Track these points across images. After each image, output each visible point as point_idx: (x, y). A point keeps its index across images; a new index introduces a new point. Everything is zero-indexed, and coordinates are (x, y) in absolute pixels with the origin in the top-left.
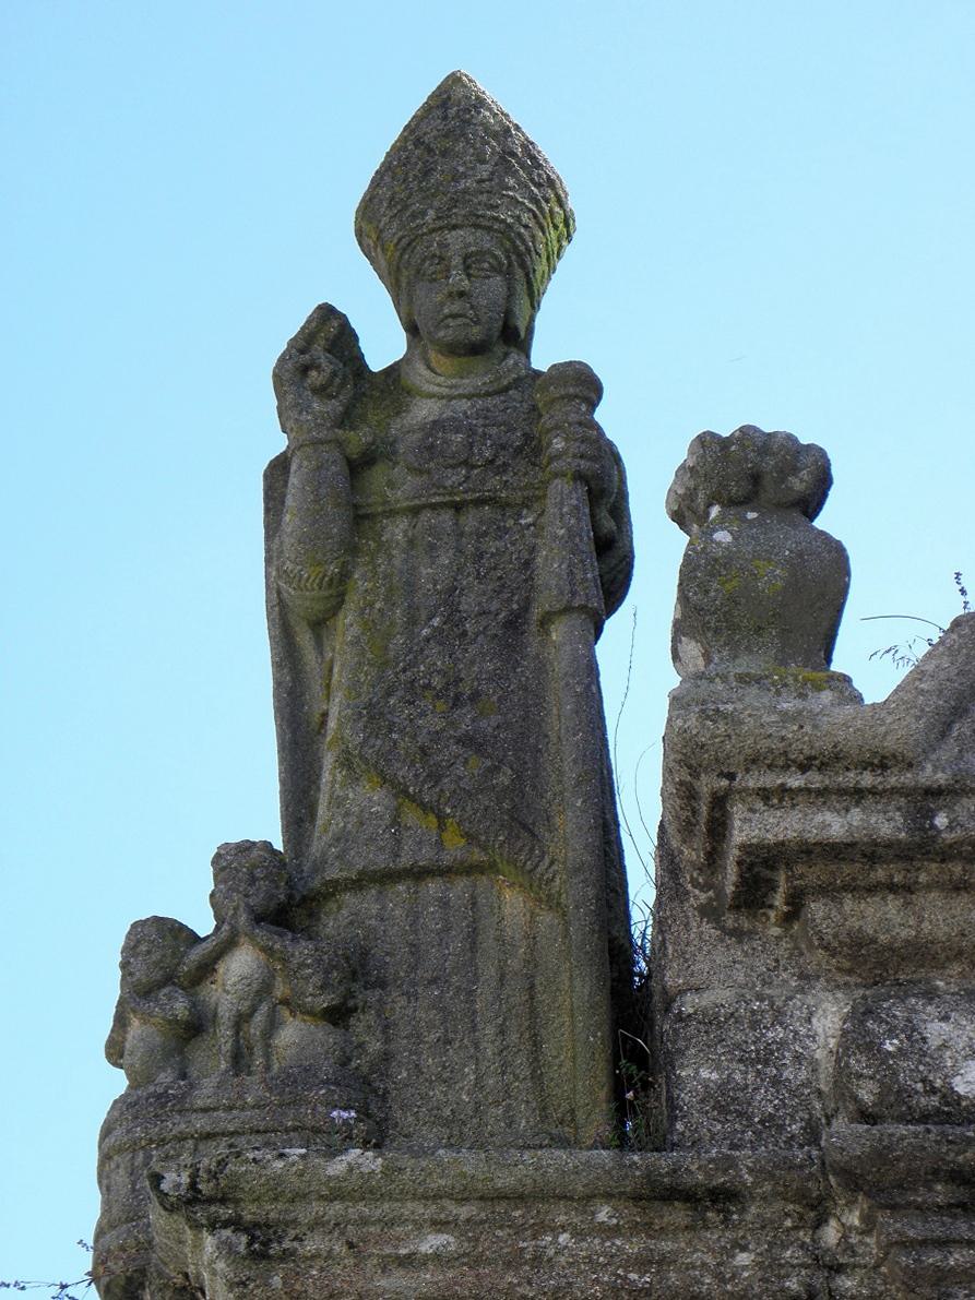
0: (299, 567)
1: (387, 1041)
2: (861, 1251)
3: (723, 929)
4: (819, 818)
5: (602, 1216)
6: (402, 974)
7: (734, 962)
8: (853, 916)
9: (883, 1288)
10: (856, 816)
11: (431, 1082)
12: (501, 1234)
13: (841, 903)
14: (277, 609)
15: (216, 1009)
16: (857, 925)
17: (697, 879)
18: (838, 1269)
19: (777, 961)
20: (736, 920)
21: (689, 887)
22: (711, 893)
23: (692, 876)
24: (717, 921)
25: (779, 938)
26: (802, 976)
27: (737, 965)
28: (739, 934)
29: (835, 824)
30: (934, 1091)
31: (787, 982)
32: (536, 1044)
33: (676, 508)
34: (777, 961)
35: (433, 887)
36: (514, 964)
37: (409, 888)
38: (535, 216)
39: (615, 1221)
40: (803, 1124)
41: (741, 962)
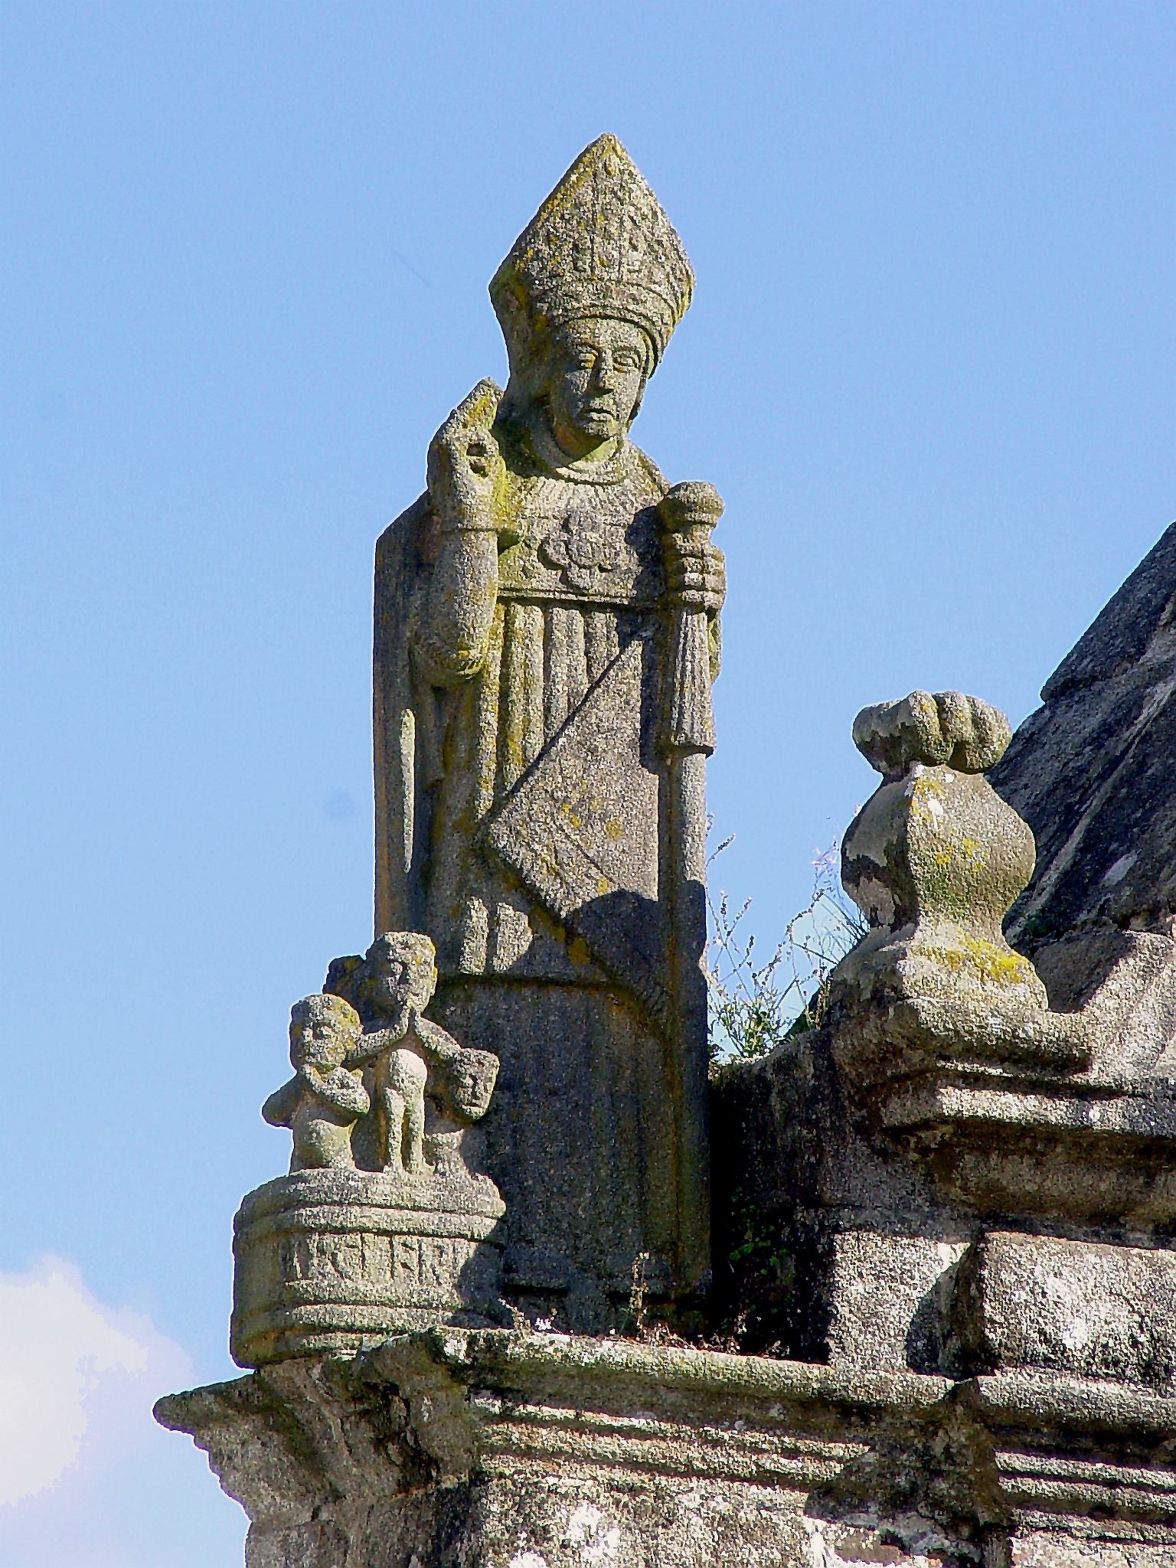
0: (447, 647)
1: (515, 1145)
2: (958, 1461)
3: (871, 1147)
4: (1003, 1099)
5: (774, 1413)
6: (527, 1080)
7: (881, 1182)
8: (994, 1170)
9: (967, 1492)
10: (1032, 1102)
11: (552, 1193)
12: (692, 1416)
13: (988, 1157)
14: (407, 669)
15: (947, 1533)
16: (997, 1177)
17: (853, 1097)
18: (938, 1473)
19: (913, 1185)
20: (883, 1142)
21: (846, 1103)
22: (864, 1112)
23: (849, 1093)
24: (868, 1140)
25: (915, 1163)
26: (933, 1203)
27: (883, 1186)
28: (883, 1154)
29: (1013, 1107)
30: (1047, 1341)
31: (921, 1207)
32: (642, 1171)
33: (868, 739)
34: (913, 1185)
35: (555, 996)
36: (622, 1087)
37: (533, 993)
38: (673, 313)
39: (782, 1416)
40: (925, 1341)
41: (885, 1182)
